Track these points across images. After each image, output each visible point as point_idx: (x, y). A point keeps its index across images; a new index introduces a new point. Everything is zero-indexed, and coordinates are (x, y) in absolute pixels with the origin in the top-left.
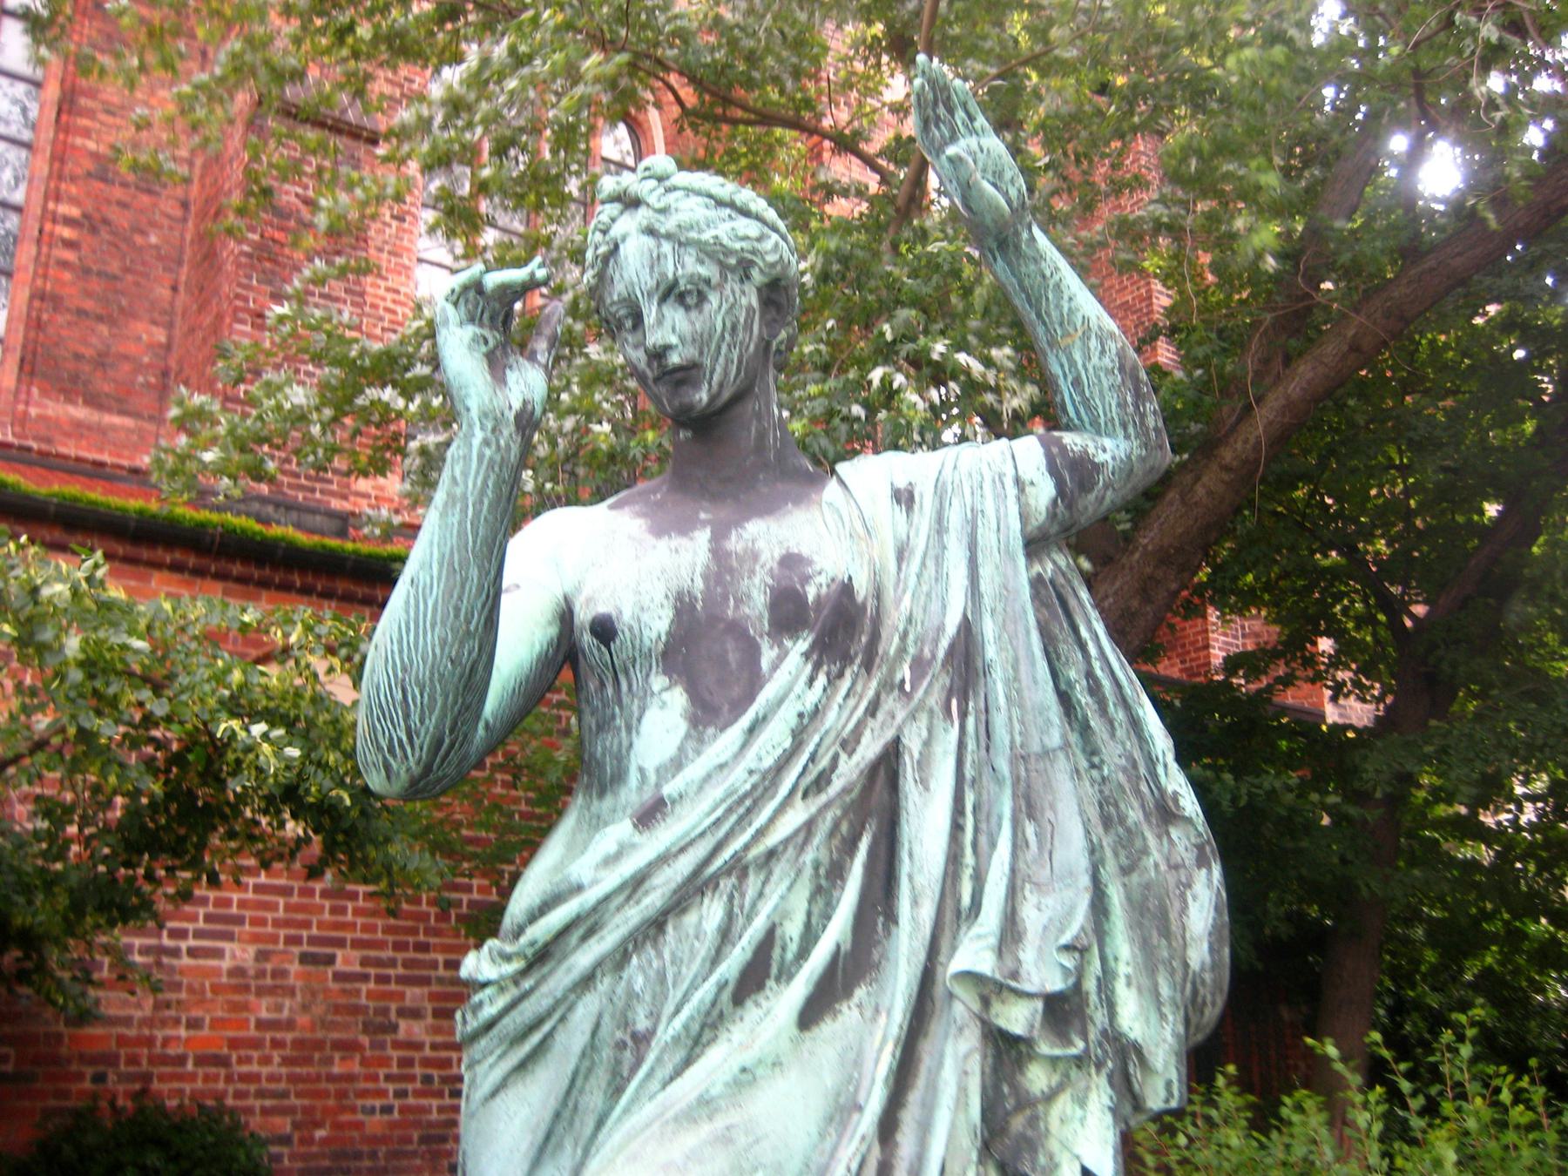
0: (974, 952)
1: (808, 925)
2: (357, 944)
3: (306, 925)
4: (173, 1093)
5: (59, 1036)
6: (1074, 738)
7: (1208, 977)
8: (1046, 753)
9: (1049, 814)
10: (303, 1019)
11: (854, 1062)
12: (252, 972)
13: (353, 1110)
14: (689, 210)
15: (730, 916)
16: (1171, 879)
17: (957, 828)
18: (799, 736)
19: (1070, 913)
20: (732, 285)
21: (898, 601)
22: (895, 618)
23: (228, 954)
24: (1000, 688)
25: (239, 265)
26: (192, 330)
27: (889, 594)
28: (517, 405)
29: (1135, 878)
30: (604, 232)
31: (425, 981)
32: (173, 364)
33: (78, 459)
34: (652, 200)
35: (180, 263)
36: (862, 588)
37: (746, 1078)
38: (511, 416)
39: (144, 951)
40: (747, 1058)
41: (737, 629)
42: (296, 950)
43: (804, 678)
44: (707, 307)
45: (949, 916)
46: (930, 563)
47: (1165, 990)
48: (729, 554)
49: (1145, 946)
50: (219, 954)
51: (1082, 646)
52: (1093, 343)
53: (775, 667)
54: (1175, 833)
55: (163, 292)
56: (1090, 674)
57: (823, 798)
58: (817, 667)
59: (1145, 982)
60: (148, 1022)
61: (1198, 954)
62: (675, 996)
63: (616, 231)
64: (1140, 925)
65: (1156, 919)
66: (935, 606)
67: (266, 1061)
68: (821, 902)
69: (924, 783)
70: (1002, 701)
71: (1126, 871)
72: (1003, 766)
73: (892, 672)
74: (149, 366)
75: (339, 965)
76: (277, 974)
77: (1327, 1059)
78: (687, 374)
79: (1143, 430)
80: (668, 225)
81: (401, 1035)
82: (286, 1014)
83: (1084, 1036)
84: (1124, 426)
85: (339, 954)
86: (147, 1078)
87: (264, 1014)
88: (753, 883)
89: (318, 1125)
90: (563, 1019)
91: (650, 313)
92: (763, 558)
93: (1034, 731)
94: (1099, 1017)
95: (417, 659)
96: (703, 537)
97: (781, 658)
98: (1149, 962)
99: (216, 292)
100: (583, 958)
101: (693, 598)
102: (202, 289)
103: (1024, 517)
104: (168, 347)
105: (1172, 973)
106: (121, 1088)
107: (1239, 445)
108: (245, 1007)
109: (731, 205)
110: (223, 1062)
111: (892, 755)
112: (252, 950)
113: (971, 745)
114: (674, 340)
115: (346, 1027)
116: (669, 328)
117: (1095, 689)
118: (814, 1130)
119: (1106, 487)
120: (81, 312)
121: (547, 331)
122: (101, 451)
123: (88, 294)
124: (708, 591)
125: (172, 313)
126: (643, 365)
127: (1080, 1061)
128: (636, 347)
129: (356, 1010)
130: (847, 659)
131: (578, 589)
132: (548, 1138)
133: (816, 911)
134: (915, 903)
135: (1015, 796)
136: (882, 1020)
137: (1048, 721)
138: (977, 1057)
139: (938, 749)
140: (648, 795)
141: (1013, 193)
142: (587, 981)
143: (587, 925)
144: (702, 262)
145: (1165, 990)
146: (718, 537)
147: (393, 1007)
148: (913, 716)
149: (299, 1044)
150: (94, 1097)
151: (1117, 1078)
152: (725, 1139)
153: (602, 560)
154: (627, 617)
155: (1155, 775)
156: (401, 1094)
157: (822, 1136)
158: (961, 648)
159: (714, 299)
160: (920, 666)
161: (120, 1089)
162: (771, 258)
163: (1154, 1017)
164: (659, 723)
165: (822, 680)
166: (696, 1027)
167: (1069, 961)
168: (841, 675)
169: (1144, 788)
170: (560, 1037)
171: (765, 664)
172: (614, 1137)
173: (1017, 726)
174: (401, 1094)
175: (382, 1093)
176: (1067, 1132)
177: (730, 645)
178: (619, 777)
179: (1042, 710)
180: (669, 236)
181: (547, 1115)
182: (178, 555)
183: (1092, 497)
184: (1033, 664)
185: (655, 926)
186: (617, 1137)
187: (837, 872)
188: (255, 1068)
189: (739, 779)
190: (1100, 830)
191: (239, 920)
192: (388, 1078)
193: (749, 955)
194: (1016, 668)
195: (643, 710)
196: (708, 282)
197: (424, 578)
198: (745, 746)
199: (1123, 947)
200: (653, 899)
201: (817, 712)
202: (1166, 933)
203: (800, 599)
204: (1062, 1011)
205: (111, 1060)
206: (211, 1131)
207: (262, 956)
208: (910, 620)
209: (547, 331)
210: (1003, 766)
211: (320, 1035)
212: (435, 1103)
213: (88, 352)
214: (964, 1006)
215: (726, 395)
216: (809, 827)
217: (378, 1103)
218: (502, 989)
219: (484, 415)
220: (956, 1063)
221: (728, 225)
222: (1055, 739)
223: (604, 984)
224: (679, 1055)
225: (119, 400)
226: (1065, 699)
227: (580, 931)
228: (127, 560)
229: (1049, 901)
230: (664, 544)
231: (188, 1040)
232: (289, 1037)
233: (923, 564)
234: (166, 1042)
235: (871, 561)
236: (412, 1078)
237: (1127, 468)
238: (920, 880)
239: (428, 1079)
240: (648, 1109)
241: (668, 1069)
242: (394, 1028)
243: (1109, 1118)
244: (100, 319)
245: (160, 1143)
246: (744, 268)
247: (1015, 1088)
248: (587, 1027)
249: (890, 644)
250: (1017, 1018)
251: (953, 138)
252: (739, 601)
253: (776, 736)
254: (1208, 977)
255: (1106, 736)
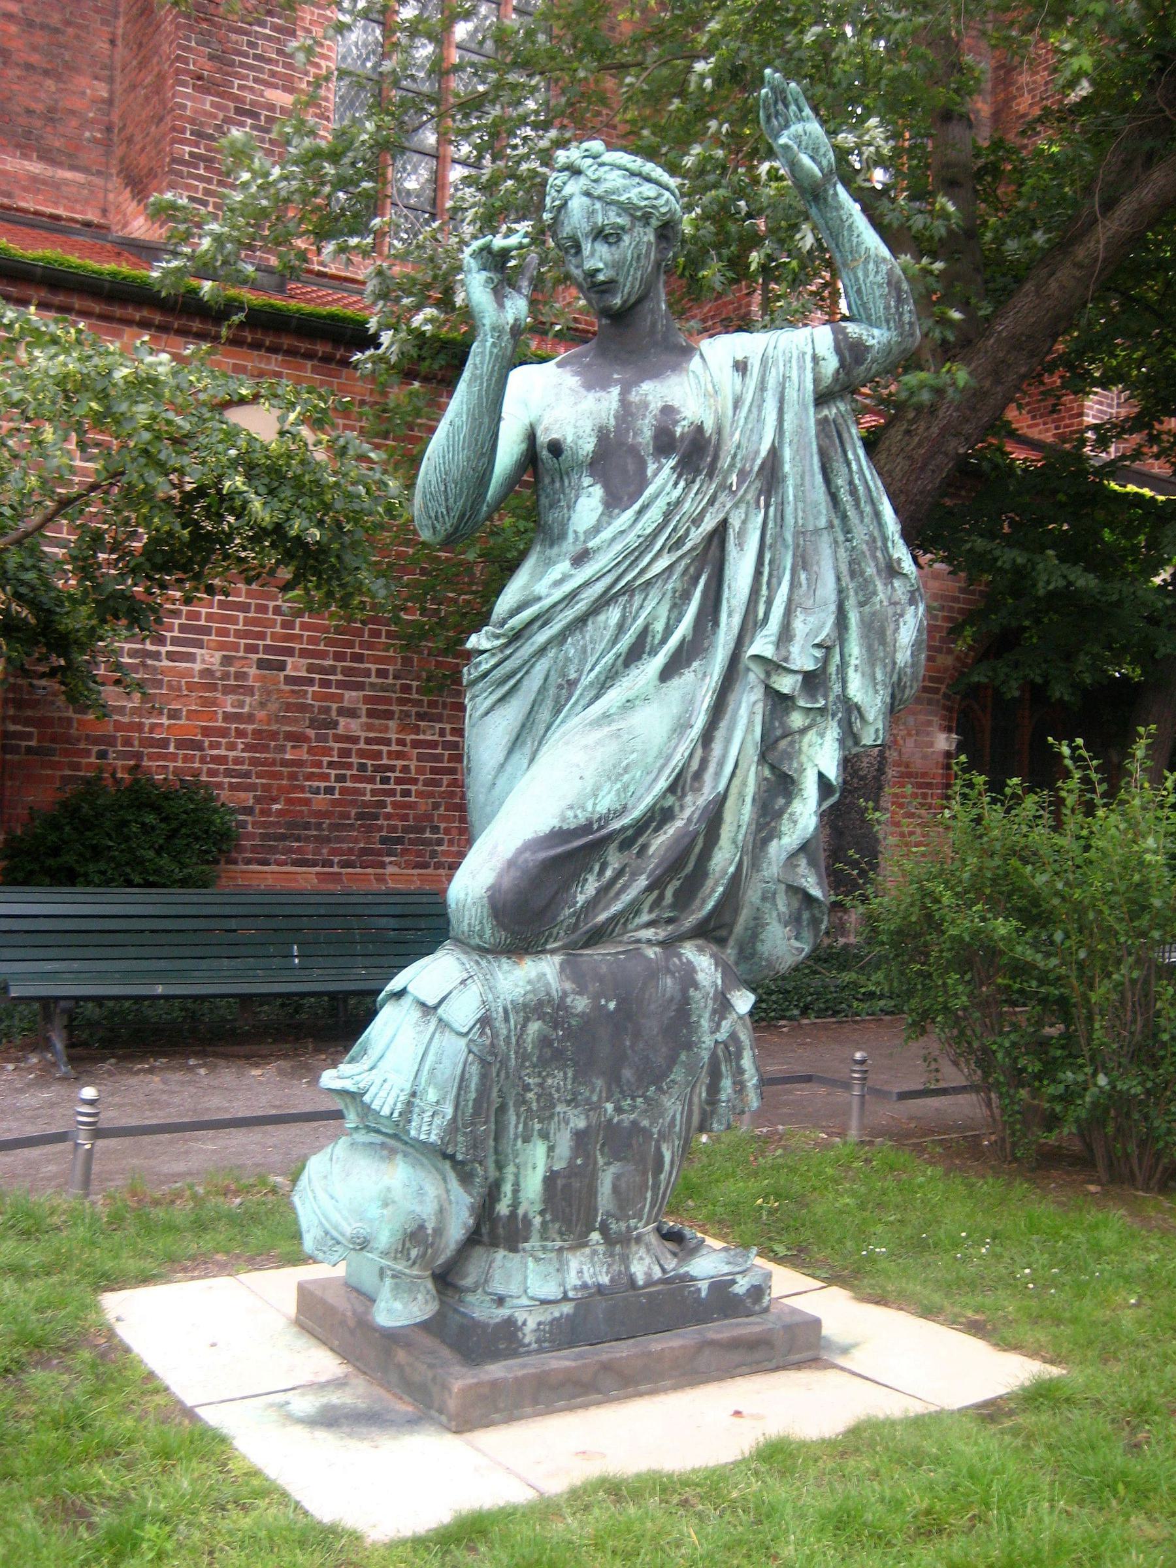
0: (762, 645)
1: (667, 624)
2: (304, 653)
3: (262, 636)
4: (162, 769)
5: (70, 720)
6: (836, 522)
7: (908, 670)
8: (817, 531)
9: (815, 568)
10: (261, 714)
11: (689, 702)
12: (218, 674)
13: (302, 789)
14: (614, 180)
15: (624, 618)
16: (890, 610)
17: (758, 573)
18: (667, 516)
19: (822, 627)
20: (639, 229)
21: (732, 435)
22: (729, 445)
23: (199, 658)
24: (791, 491)
25: (178, 27)
26: (133, 87)
27: (727, 431)
28: (511, 321)
29: (867, 609)
30: (559, 192)
31: (359, 687)
32: (115, 118)
33: (36, 213)
34: (589, 173)
35: (116, 16)
36: (709, 427)
37: (629, 705)
38: (508, 328)
39: (133, 654)
40: (630, 695)
41: (634, 451)
42: (255, 656)
43: (671, 483)
44: (622, 244)
45: (751, 624)
46: (755, 410)
47: (879, 676)
48: (630, 403)
49: (870, 650)
50: (191, 658)
51: (849, 464)
52: (871, 266)
53: (655, 475)
54: (897, 583)
55: (102, 46)
56: (851, 483)
57: (680, 553)
58: (679, 476)
59: (867, 670)
60: (135, 711)
61: (903, 657)
62: (591, 660)
63: (567, 191)
64: (867, 637)
65: (878, 634)
66: (755, 438)
67: (232, 747)
68: (676, 612)
69: (740, 546)
70: (791, 498)
71: (862, 604)
72: (789, 537)
73: (725, 478)
74: (93, 121)
75: (289, 672)
76: (240, 676)
77: (1060, 756)
78: (608, 287)
79: (900, 325)
80: (599, 190)
81: (340, 730)
82: (246, 709)
83: (826, 697)
84: (888, 321)
85: (290, 660)
86: (138, 756)
87: (229, 709)
88: (637, 599)
89: (275, 800)
90: (527, 672)
91: (587, 247)
92: (652, 407)
93: (811, 518)
94: (837, 688)
95: (454, 468)
96: (615, 391)
97: (659, 469)
98: (871, 658)
99: (156, 50)
100: (541, 638)
101: (609, 431)
102: (140, 45)
103: (816, 381)
104: (110, 102)
105: (885, 666)
106: (120, 763)
107: (1092, 245)
108: (214, 703)
109: (639, 175)
110: (198, 746)
111: (722, 528)
112: (218, 655)
113: (771, 525)
114: (601, 265)
115: (296, 721)
116: (597, 257)
117: (853, 492)
118: (665, 735)
119: (873, 361)
120: (29, 67)
121: (528, 275)
122: (56, 204)
123: (34, 48)
124: (617, 426)
125: (111, 68)
126: (581, 279)
127: (822, 711)
128: (577, 267)
129: (303, 708)
130: (698, 472)
131: (539, 421)
132: (517, 739)
133: (673, 617)
134: (730, 615)
135: (794, 555)
136: (708, 680)
137: (819, 512)
138: (761, 704)
139: (750, 526)
140: (579, 548)
141: (825, 163)
142: (542, 651)
143: (543, 619)
144: (619, 215)
145: (879, 676)
146: (624, 393)
147: (335, 706)
148: (736, 506)
149: (257, 733)
150: (100, 769)
151: (845, 723)
152: (617, 735)
153: (552, 400)
154: (569, 440)
155: (887, 548)
156: (341, 778)
157: (669, 739)
158: (769, 464)
159: (626, 238)
160: (742, 475)
161: (120, 766)
162: (663, 210)
163: (871, 691)
164: (587, 505)
165: (682, 484)
166: (603, 678)
167: (819, 653)
168: (693, 481)
169: (879, 554)
170: (525, 682)
171: (649, 473)
172: (555, 736)
173: (800, 514)
174: (341, 778)
175: (325, 777)
176: (812, 751)
177: (629, 460)
178: (563, 536)
179: (816, 505)
180: (599, 198)
181: (518, 724)
182: (145, 313)
183: (863, 368)
184: (813, 475)
185: (581, 621)
186: (557, 735)
187: (686, 596)
188: (222, 752)
189: (631, 539)
190: (848, 579)
191: (206, 631)
192: (331, 765)
193: (633, 640)
194: (802, 478)
195: (577, 497)
196: (622, 228)
197: (457, 422)
198: (635, 521)
199: (855, 649)
200: (581, 607)
201: (679, 502)
202: (883, 643)
203: (671, 434)
204: (812, 681)
205: (110, 741)
206: (191, 800)
207: (227, 661)
208: (738, 447)
209: (528, 275)
210: (789, 537)
211: (274, 727)
212: (369, 786)
213: (39, 107)
214: (755, 675)
215: (632, 300)
216: (670, 568)
217: (323, 785)
218: (493, 655)
219: (493, 329)
220: (748, 707)
221: (637, 190)
222: (822, 522)
223: (551, 653)
224: (593, 693)
225: (69, 156)
226: (834, 497)
227: (539, 623)
228: (103, 317)
229: (811, 619)
230: (591, 396)
231: (169, 726)
232: (251, 727)
233: (750, 411)
234: (153, 727)
235: (716, 411)
236: (349, 766)
237: (888, 349)
238: (734, 602)
239: (362, 767)
240: (575, 720)
241: (583, 702)
242: (335, 725)
243: (836, 745)
244: (46, 73)
245: (155, 808)
246: (646, 218)
247: (782, 724)
248: (542, 676)
249: (725, 462)
250: (786, 684)
251: (787, 126)
252: (635, 434)
253: (654, 515)
254: (908, 670)
255: (857, 522)
